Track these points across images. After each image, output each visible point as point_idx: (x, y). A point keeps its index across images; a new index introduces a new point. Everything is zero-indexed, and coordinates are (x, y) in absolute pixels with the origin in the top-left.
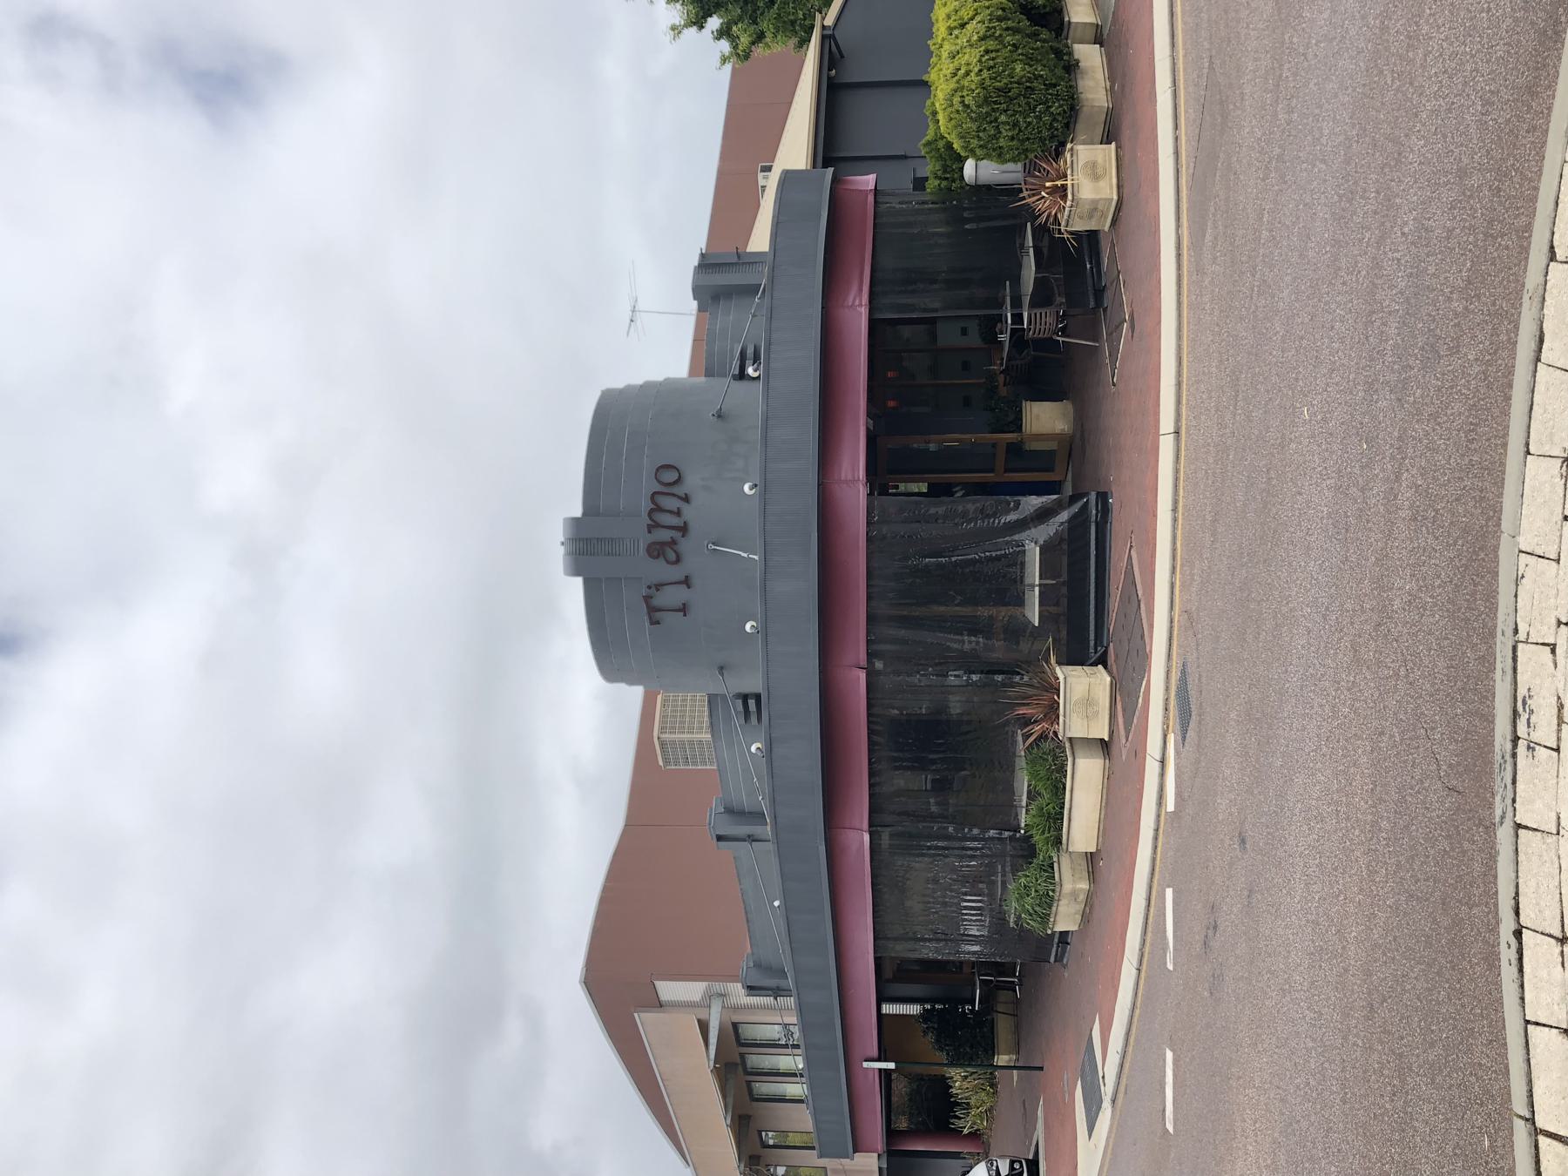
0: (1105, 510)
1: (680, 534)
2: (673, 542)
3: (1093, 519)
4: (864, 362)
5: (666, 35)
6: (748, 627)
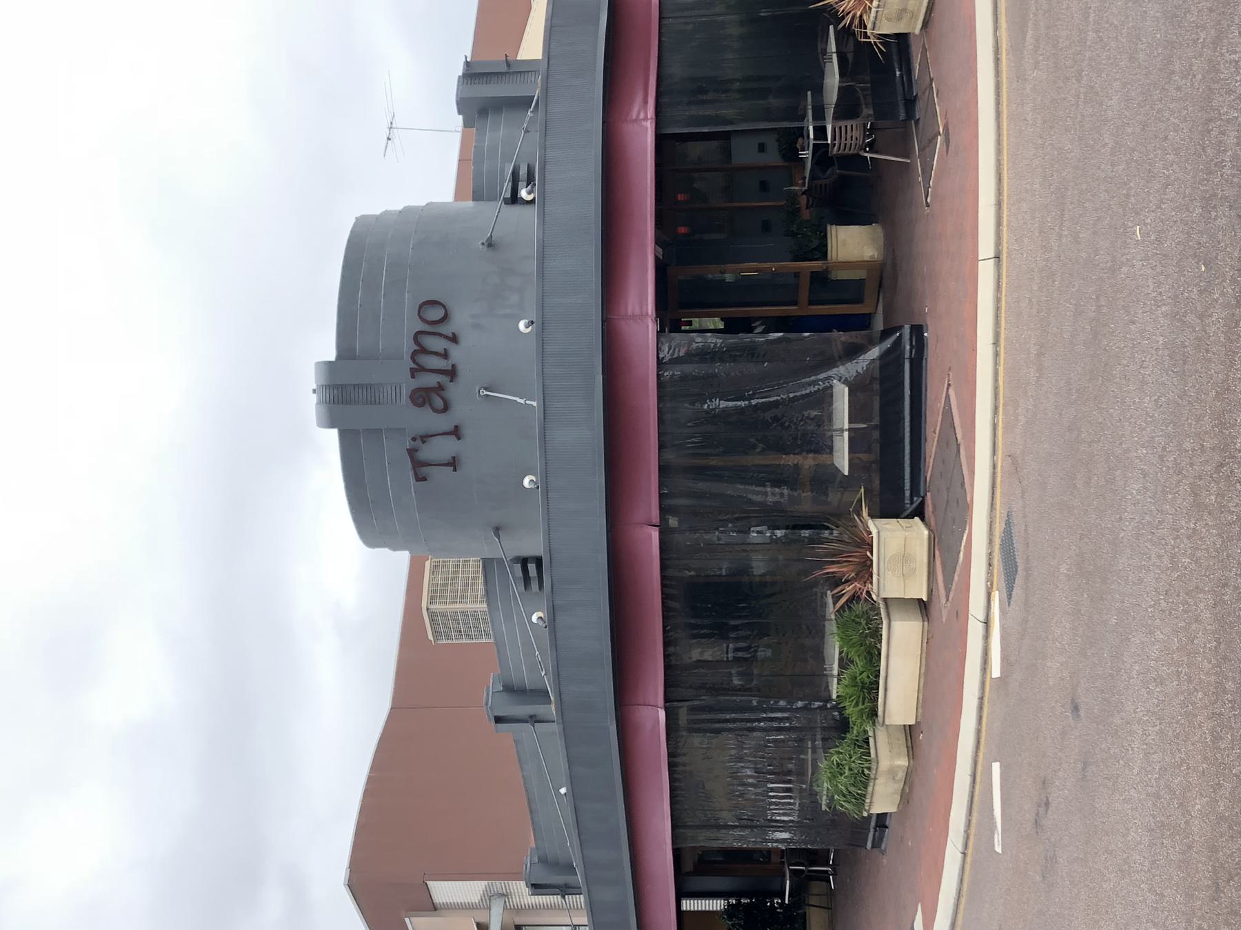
2: (440, 388)
3: (907, 355)
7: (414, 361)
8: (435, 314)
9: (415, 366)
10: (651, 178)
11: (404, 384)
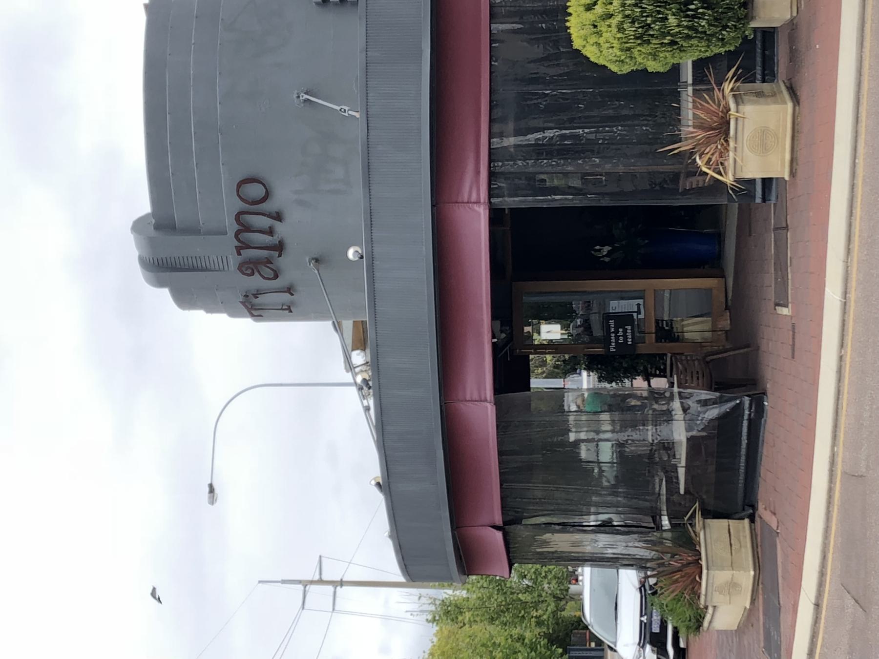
0: (760, 410)
1: (276, 254)
2: (268, 261)
3: (746, 417)
4: (487, 294)
5: (258, 297)
6: (351, 254)
7: (239, 240)
8: (255, 190)
9: (240, 244)
10: (486, 287)
11: (230, 256)
